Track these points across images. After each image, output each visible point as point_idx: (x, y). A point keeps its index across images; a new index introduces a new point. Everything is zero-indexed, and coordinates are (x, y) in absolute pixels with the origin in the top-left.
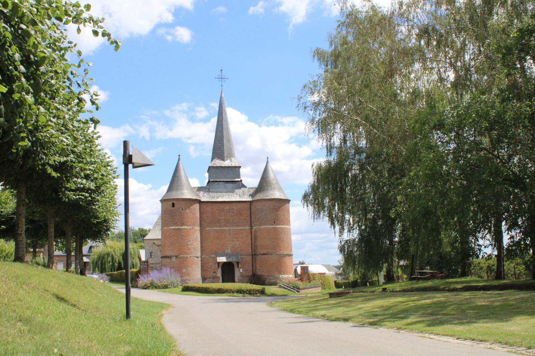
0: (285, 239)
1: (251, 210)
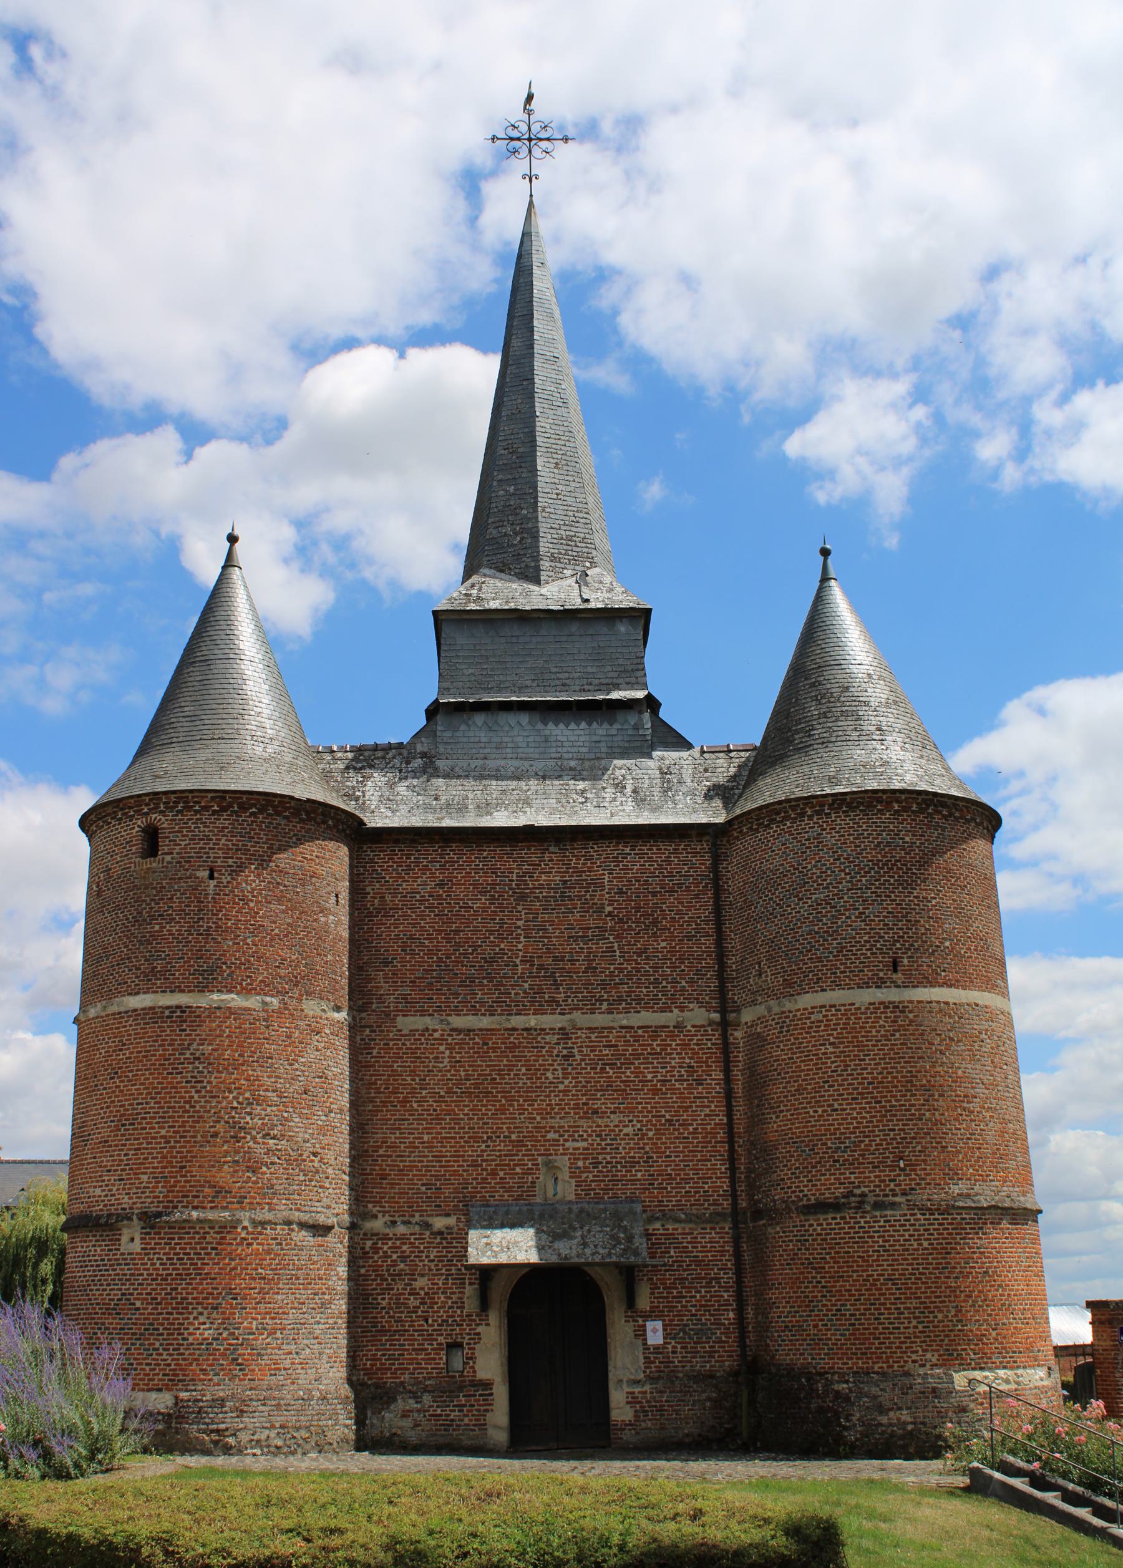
0: (980, 1090)
1: (718, 890)
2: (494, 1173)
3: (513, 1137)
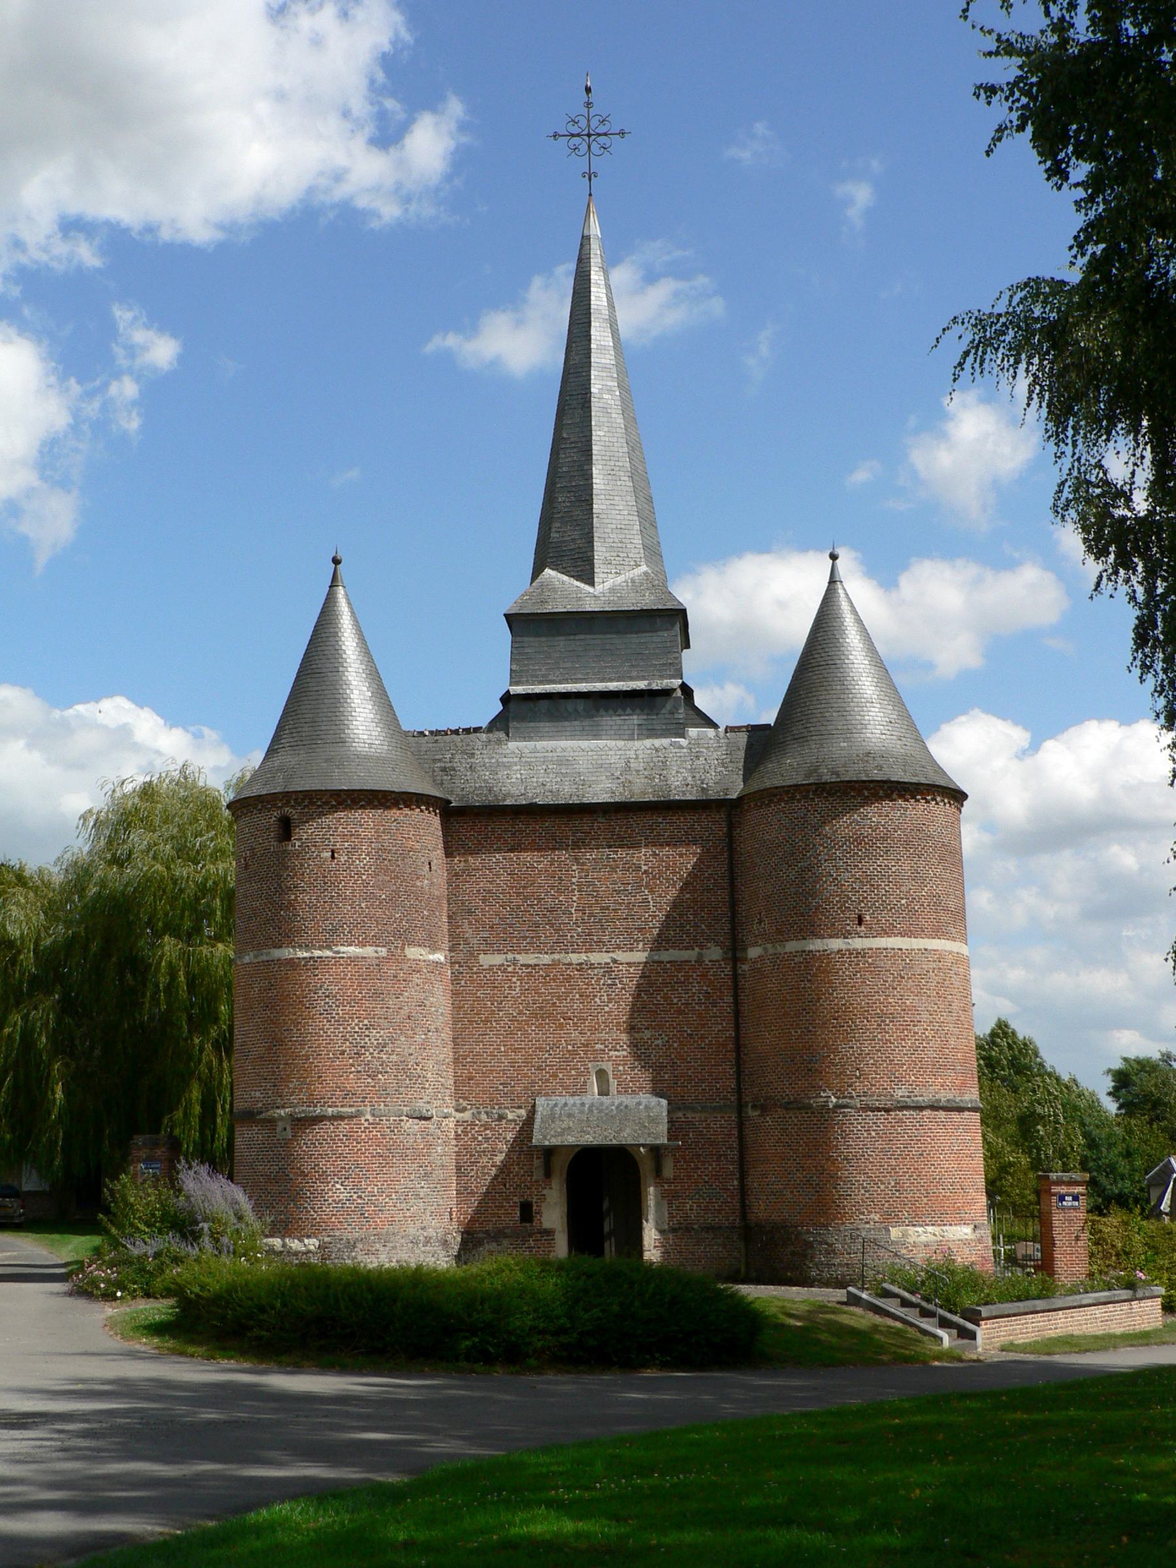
2: (555, 1076)
3: (570, 1047)
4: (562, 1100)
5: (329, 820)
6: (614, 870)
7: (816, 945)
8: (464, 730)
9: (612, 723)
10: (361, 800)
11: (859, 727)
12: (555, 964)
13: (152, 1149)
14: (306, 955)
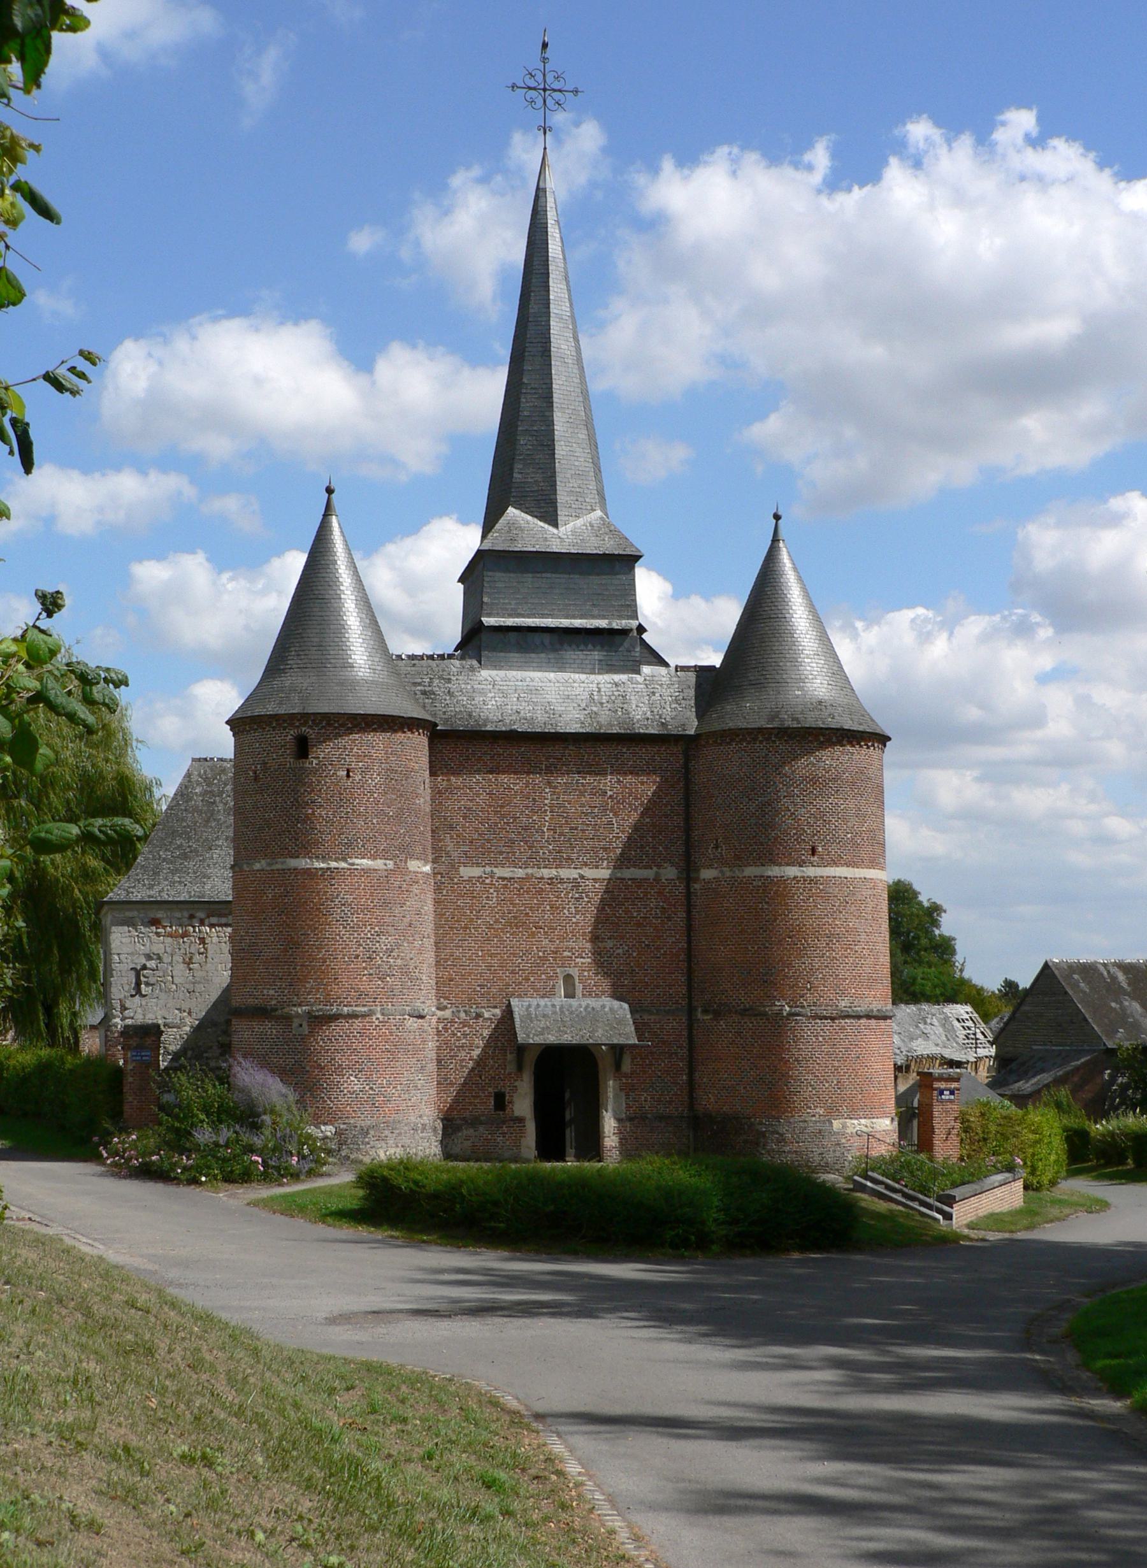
2: (527, 979)
3: (541, 954)
4: (534, 1002)
5: (344, 741)
6: (582, 794)
7: (774, 871)
8: (438, 655)
9: (576, 657)
10: (374, 723)
11: (810, 677)
12: (528, 877)
13: (141, 1038)
14: (322, 865)
